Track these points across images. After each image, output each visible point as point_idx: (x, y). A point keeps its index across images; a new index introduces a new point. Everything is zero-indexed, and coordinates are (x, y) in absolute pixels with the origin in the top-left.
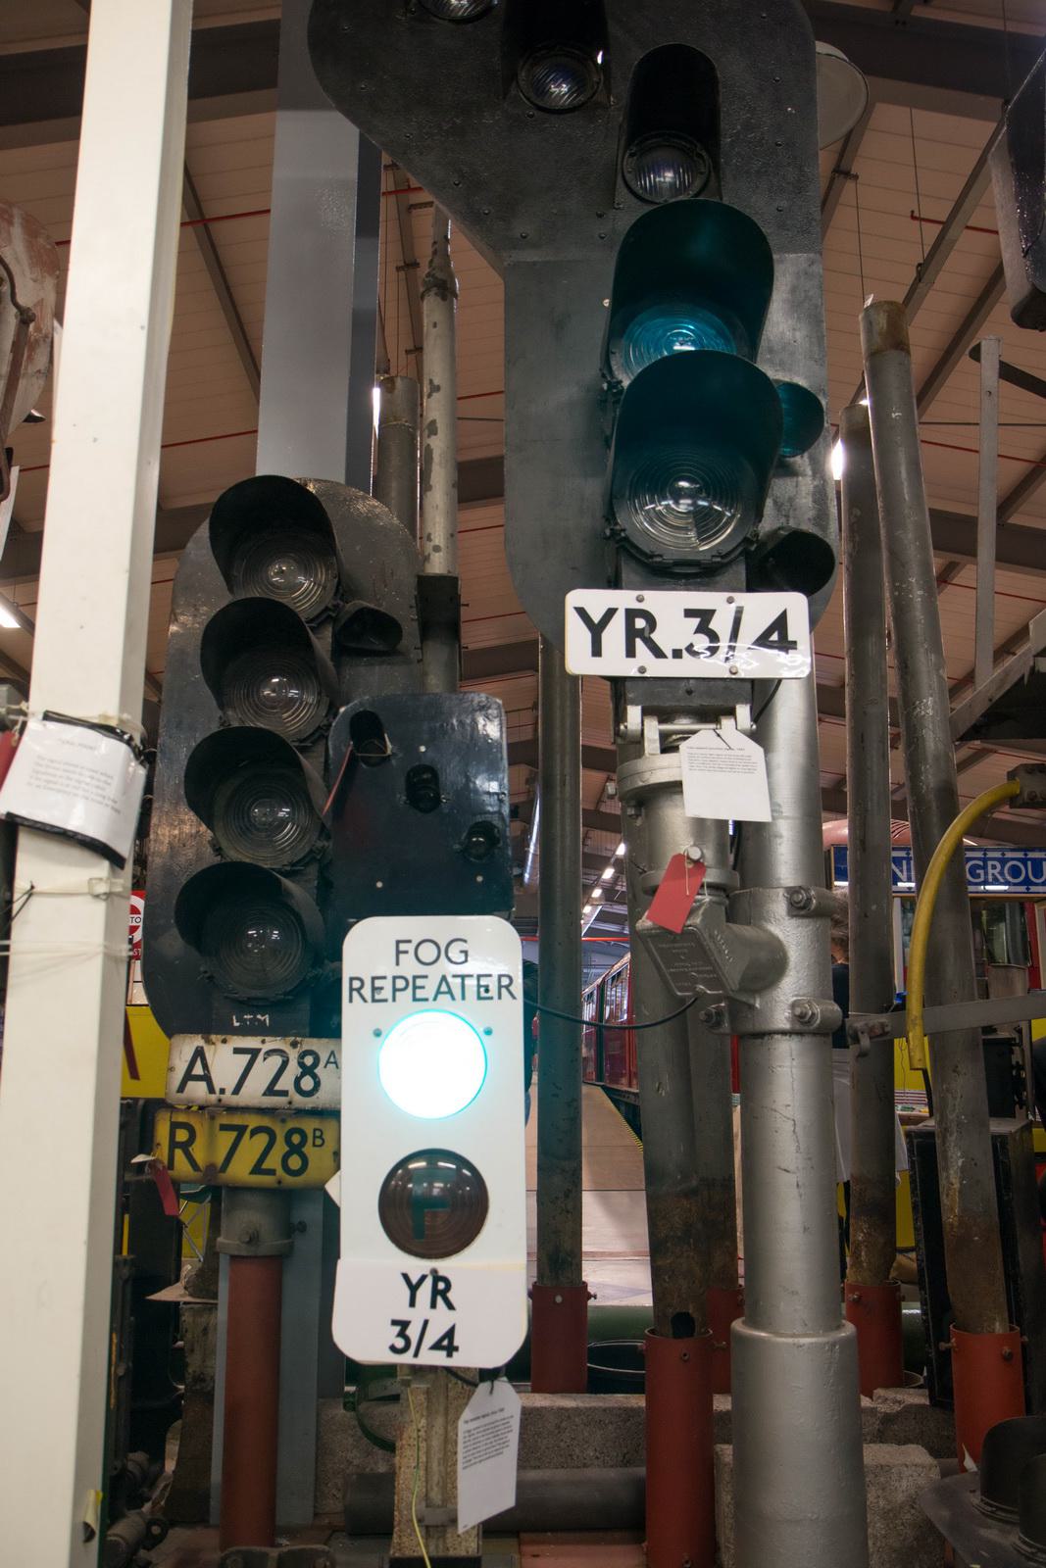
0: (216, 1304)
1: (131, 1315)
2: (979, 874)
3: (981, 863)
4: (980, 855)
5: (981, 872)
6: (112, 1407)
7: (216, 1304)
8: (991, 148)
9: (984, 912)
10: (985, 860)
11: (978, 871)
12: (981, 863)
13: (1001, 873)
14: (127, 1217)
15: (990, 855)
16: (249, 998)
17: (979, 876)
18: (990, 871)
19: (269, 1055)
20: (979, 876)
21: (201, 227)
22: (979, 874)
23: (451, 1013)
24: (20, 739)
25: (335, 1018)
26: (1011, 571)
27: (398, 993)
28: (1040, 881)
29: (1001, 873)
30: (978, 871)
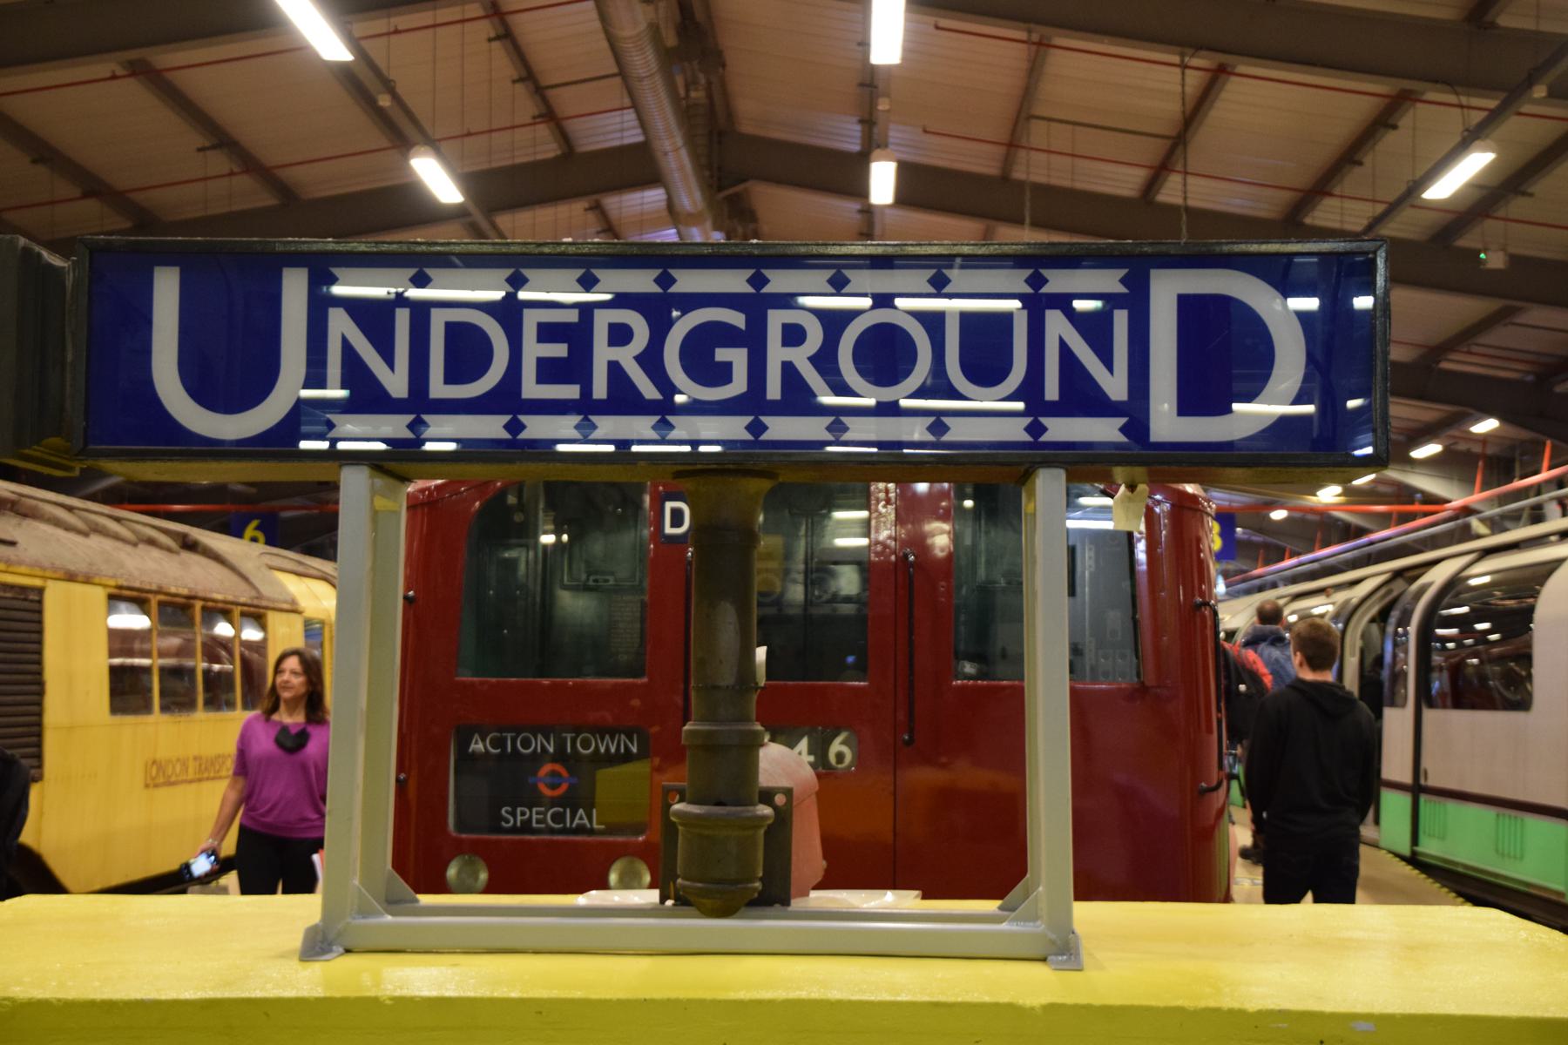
0: (112, 654)
1: (1515, 260)
2: (728, 366)
3: (737, 319)
4: (735, 281)
5: (738, 358)
6: (830, 449)
7: (112, 654)
9: (645, 680)
10: (756, 305)
11: (722, 354)
12: (737, 319)
13: (651, 360)
14: (611, 448)
17: (722, 374)
18: (777, 354)
20: (722, 374)
21: (496, 20)
22: (728, 366)
25: (1478, 414)
26: (1034, 625)
29: (651, 360)
30: (722, 354)
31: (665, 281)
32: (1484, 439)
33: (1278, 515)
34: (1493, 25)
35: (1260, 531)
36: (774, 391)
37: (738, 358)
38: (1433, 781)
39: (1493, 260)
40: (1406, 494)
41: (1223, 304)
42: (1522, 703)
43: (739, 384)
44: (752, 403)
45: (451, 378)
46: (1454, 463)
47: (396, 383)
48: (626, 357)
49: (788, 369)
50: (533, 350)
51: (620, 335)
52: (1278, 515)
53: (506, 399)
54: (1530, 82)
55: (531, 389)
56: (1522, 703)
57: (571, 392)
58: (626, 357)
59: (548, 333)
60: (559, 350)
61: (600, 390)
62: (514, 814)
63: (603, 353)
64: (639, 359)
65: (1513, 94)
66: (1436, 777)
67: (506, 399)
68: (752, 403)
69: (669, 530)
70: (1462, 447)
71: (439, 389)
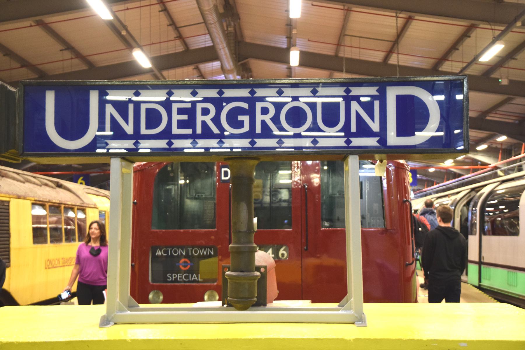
2: (243, 122)
3: (245, 106)
4: (244, 93)
5: (246, 119)
8: (118, 85)
9: (216, 230)
10: (252, 101)
11: (240, 118)
12: (245, 106)
13: (216, 120)
15: (229, 93)
16: (41, 186)
17: (241, 124)
18: (259, 117)
19: (38, 25)
20: (241, 124)
22: (243, 122)
23: (306, 212)
24: (34, 170)
27: (203, 21)
28: (256, 193)
29: (216, 120)
30: (240, 118)
31: (221, 93)
32: (501, 143)
33: (431, 170)
34: (438, 71)
35: (425, 175)
36: (258, 130)
37: (246, 119)
38: (486, 260)
39: (504, 82)
40: (475, 162)
41: (412, 98)
42: (516, 233)
43: (246, 128)
44: (251, 134)
45: (148, 127)
46: (492, 151)
47: (129, 129)
48: (208, 119)
49: (204, 123)
50: (176, 118)
51: (205, 112)
52: (431, 170)
53: (167, 134)
54: (515, 20)
55: (175, 130)
56: (516, 233)
57: (189, 131)
58: (208, 119)
59: (181, 111)
60: (185, 117)
61: (199, 131)
62: (172, 276)
63: (200, 118)
64: (212, 120)
65: (510, 25)
66: (487, 259)
67: (167, 134)
68: (251, 134)
69: (223, 178)
70: (494, 146)
71: (144, 131)
